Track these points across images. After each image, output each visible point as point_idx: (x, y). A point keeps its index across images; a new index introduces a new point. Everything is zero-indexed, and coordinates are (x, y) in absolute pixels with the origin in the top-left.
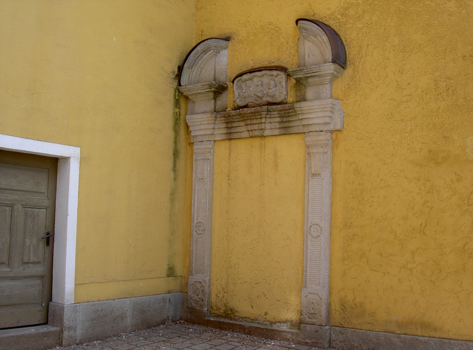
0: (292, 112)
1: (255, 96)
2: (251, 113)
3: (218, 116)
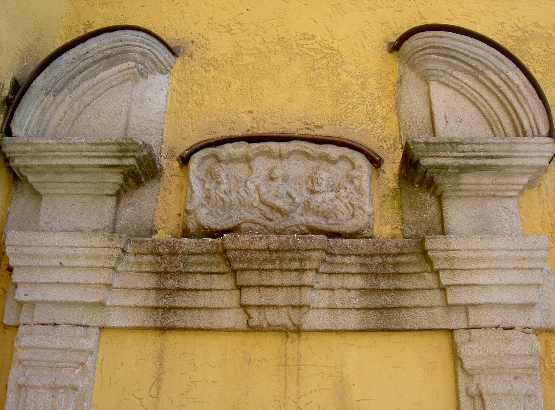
0: (408, 264)
1: (262, 207)
2: (268, 249)
3: (129, 249)
